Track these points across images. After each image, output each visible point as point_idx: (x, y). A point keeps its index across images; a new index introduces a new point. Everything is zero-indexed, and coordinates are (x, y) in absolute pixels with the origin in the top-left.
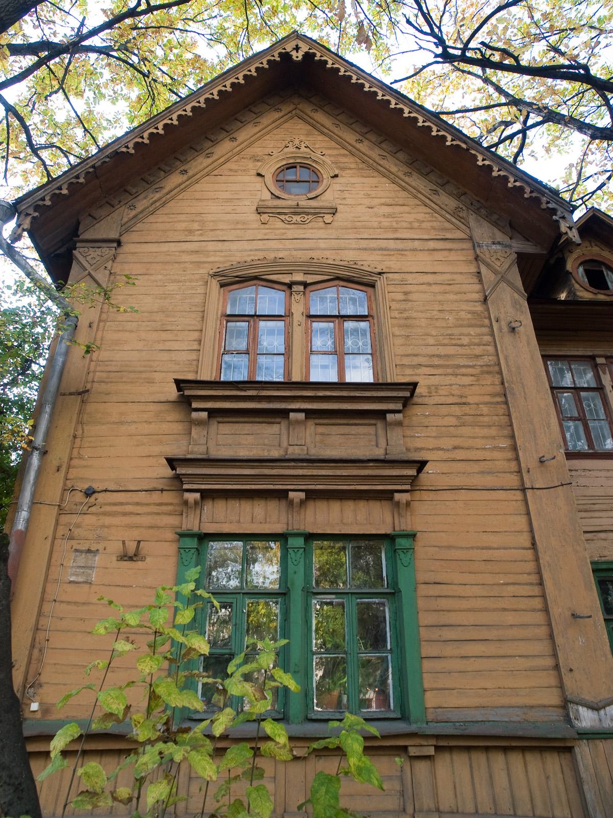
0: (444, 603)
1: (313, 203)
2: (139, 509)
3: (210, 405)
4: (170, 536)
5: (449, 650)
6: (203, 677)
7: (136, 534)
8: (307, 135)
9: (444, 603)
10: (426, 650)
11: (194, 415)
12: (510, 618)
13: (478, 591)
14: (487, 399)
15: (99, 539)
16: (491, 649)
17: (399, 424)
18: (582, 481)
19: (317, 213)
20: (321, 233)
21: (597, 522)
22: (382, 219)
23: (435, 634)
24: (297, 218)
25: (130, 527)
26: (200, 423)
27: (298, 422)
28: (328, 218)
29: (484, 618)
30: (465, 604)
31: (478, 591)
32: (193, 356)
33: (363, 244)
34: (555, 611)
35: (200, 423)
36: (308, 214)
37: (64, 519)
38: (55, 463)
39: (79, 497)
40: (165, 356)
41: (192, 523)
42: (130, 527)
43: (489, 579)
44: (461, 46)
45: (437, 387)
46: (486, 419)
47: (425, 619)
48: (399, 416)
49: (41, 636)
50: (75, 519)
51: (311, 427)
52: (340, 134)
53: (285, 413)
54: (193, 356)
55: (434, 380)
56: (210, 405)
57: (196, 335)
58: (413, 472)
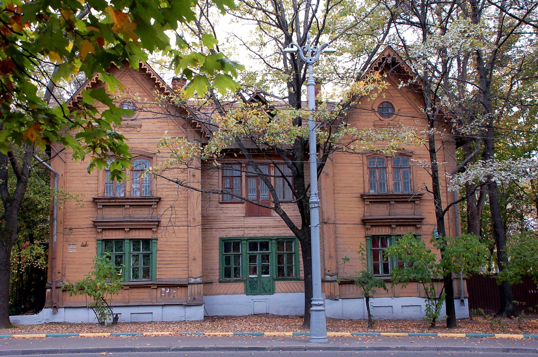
0: (163, 255)
1: (133, 122)
2: (85, 233)
3: (103, 204)
4: (94, 240)
5: (163, 266)
6: (522, 46)
7: (85, 240)
8: (132, 84)
9: (163, 255)
10: (158, 266)
11: (98, 207)
12: (179, 259)
13: (172, 252)
14: (183, 199)
15: (76, 241)
16: (168, 266)
17: (155, 208)
18: (225, 211)
19: (134, 127)
20: (136, 136)
21: (230, 225)
22: (157, 129)
23: (161, 262)
24: (128, 129)
25: (83, 238)
26: (99, 209)
27: (127, 208)
28: (138, 129)
29: (173, 259)
30: (168, 256)
31: (172, 252)
32: (96, 186)
33: (150, 141)
34: (190, 257)
35: (99, 209)
36: (132, 127)
37: (65, 236)
38: (60, 221)
39: (68, 230)
40: (87, 185)
41: (100, 237)
42: (83, 238)
43: (175, 249)
44: (109, 305)
45: (168, 195)
46: (181, 205)
47: (158, 259)
48: (156, 206)
49: (64, 265)
50: (68, 236)
51: (131, 209)
52: (144, 84)
53: (124, 206)
54: (96, 186)
55: (168, 193)
56: (103, 204)
57: (96, 178)
58: (157, 223)
